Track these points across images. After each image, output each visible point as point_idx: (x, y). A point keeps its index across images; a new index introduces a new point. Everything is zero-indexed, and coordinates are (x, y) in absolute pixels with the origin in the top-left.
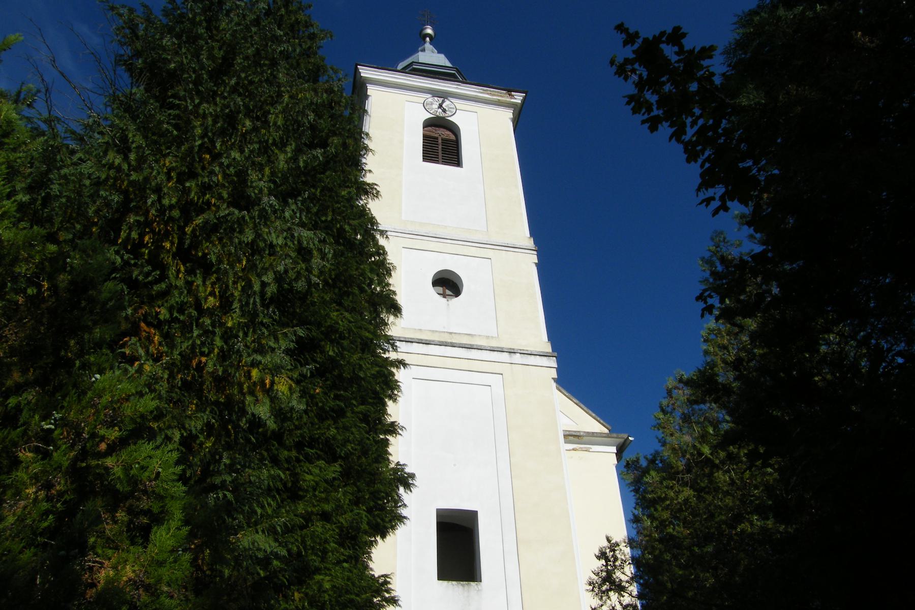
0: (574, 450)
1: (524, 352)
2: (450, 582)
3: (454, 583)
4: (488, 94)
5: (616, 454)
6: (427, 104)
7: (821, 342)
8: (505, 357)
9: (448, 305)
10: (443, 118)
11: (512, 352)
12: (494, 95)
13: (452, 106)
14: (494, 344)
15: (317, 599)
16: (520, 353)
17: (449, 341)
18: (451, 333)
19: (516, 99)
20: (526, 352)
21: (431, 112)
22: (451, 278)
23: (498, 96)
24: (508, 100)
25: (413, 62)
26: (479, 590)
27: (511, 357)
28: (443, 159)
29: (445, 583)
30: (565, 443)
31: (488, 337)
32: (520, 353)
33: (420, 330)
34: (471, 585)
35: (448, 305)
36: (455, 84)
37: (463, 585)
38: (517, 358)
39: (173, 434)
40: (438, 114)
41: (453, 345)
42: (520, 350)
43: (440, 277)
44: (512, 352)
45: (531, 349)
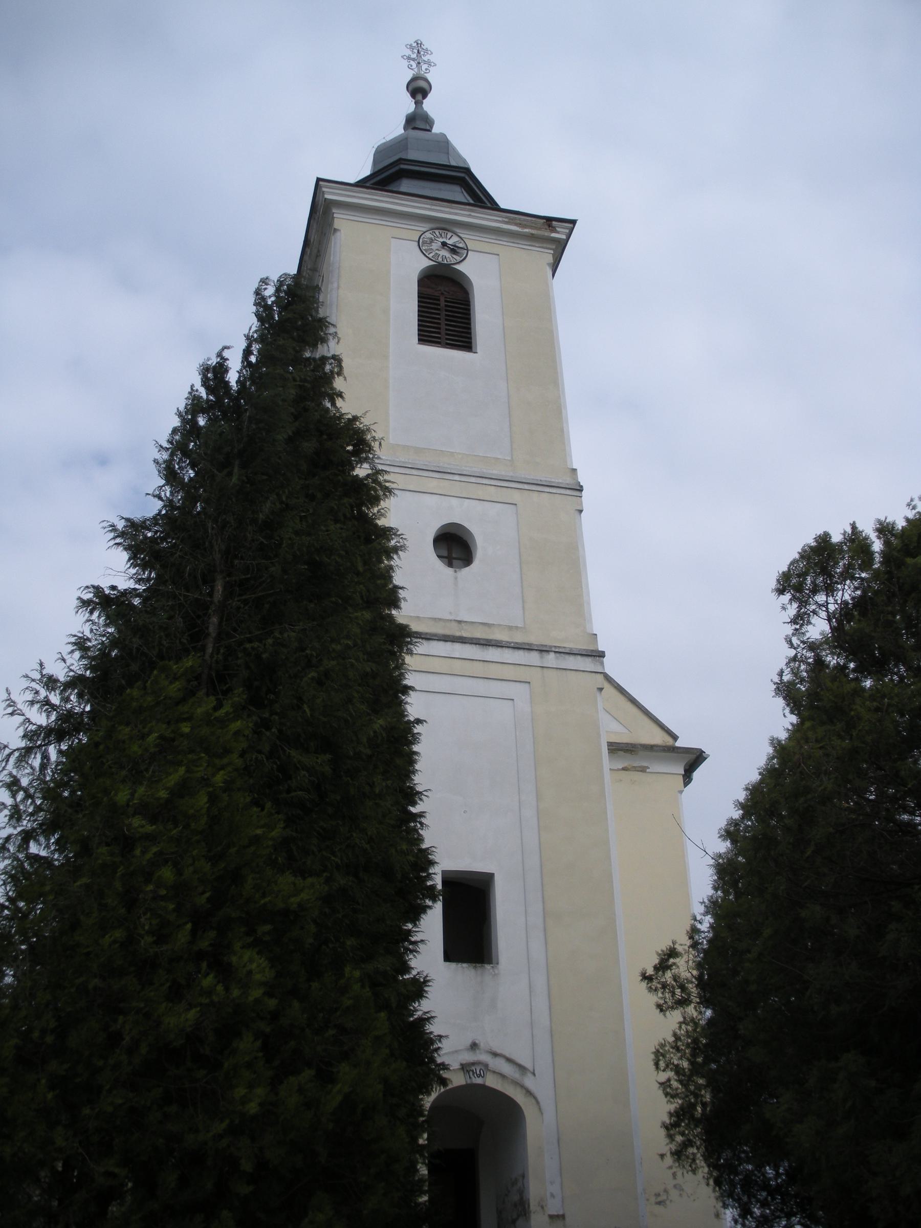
0: (624, 769)
1: (561, 650)
2: (460, 965)
3: (465, 965)
4: (516, 224)
5: (683, 776)
6: (424, 243)
7: (749, 1217)
8: (534, 658)
9: (456, 578)
10: (448, 266)
11: (543, 650)
12: (525, 226)
13: (461, 245)
14: (519, 638)
15: (81, 710)
16: (555, 652)
17: (458, 634)
18: (460, 622)
19: (558, 232)
20: (563, 650)
21: (430, 256)
22: (459, 533)
23: (531, 227)
24: (546, 234)
25: (400, 159)
26: (495, 975)
27: (542, 657)
28: (447, 320)
29: (453, 965)
30: (604, 652)
31: (510, 628)
32: (555, 652)
33: (418, 617)
34: (484, 966)
35: (456, 578)
36: (465, 210)
37: (475, 967)
38: (551, 659)
39: (169, 866)
40: (440, 259)
41: (462, 640)
42: (555, 646)
43: (443, 532)
44: (543, 650)
45: (570, 645)
